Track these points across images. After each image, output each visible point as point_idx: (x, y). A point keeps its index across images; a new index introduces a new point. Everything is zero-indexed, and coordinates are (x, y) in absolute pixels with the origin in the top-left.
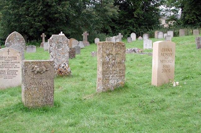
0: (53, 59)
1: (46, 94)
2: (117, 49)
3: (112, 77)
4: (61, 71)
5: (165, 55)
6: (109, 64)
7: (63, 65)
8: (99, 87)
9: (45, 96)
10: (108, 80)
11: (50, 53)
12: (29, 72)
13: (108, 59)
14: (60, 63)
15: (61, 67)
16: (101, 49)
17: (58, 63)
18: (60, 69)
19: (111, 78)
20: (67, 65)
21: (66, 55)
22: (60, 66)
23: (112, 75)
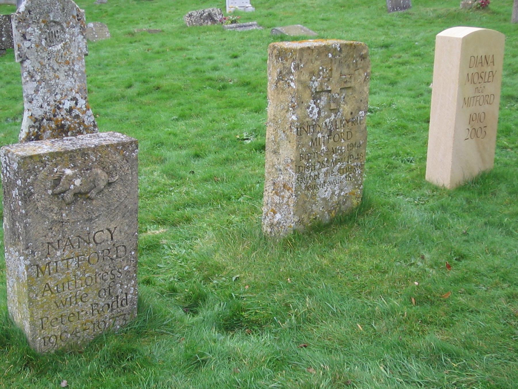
0: (35, 84)
1: (108, 277)
2: (345, 71)
3: (326, 174)
4: (63, 126)
5: (476, 80)
6: (318, 129)
7: (68, 104)
8: (278, 216)
9: (106, 286)
10: (315, 187)
11: (22, 62)
12: (42, 199)
13: (316, 110)
14: (58, 97)
15: (63, 113)
16: (290, 73)
17: (51, 99)
18: (59, 117)
19: (322, 180)
20: (82, 102)
21: (76, 68)
22: (59, 108)
23: (324, 170)
